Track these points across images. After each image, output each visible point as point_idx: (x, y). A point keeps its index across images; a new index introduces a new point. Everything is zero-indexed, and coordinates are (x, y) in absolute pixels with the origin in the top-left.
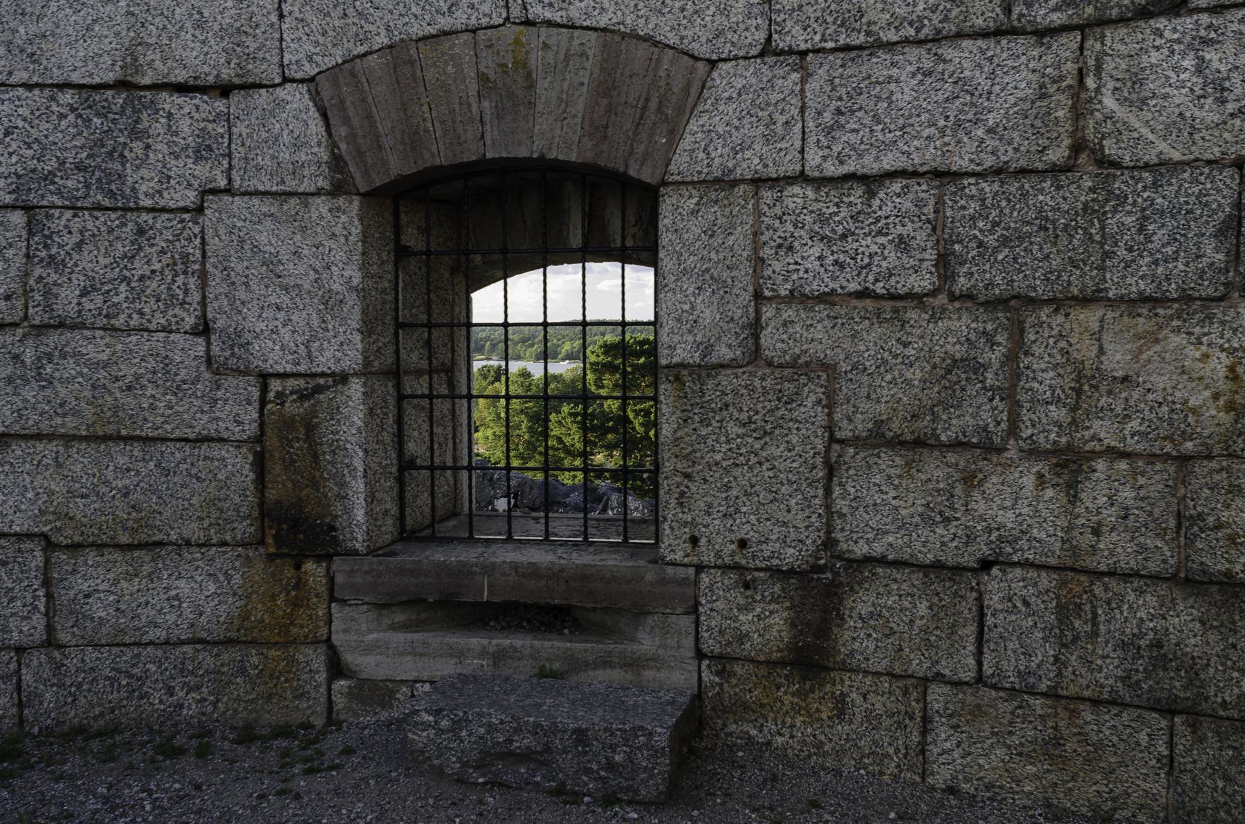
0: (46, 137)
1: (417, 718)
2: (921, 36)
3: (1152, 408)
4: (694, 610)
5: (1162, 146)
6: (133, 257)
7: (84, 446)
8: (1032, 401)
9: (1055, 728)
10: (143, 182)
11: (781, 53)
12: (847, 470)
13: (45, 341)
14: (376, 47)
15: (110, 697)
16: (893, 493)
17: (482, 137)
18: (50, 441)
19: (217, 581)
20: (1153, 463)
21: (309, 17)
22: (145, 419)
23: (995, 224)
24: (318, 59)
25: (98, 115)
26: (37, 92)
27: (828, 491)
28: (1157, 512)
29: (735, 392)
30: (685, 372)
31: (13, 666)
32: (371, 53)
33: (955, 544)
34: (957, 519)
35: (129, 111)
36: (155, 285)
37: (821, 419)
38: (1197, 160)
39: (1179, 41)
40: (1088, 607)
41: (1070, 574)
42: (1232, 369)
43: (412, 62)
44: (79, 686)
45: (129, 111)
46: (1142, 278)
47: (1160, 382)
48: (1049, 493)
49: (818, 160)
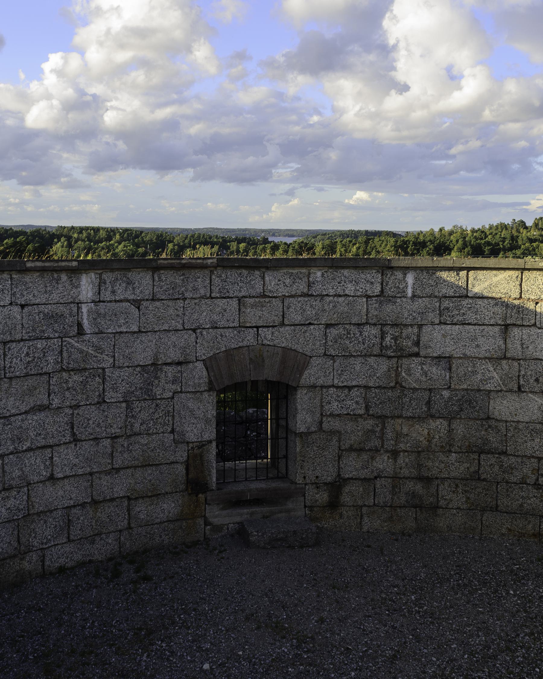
1: (252, 534)
2: (362, 355)
4: (304, 496)
5: (414, 385)
9: (391, 514)
10: (158, 392)
11: (328, 355)
13: (130, 439)
16: (354, 462)
18: (131, 468)
19: (175, 503)
21: (204, 343)
22: (157, 459)
23: (379, 399)
24: (206, 354)
25: (146, 373)
26: (130, 368)
27: (339, 462)
29: (316, 439)
30: (303, 434)
31: (118, 536)
36: (160, 420)
37: (337, 445)
39: (418, 363)
40: (399, 486)
42: (428, 433)
47: (414, 435)
48: (390, 460)
49: (337, 382)
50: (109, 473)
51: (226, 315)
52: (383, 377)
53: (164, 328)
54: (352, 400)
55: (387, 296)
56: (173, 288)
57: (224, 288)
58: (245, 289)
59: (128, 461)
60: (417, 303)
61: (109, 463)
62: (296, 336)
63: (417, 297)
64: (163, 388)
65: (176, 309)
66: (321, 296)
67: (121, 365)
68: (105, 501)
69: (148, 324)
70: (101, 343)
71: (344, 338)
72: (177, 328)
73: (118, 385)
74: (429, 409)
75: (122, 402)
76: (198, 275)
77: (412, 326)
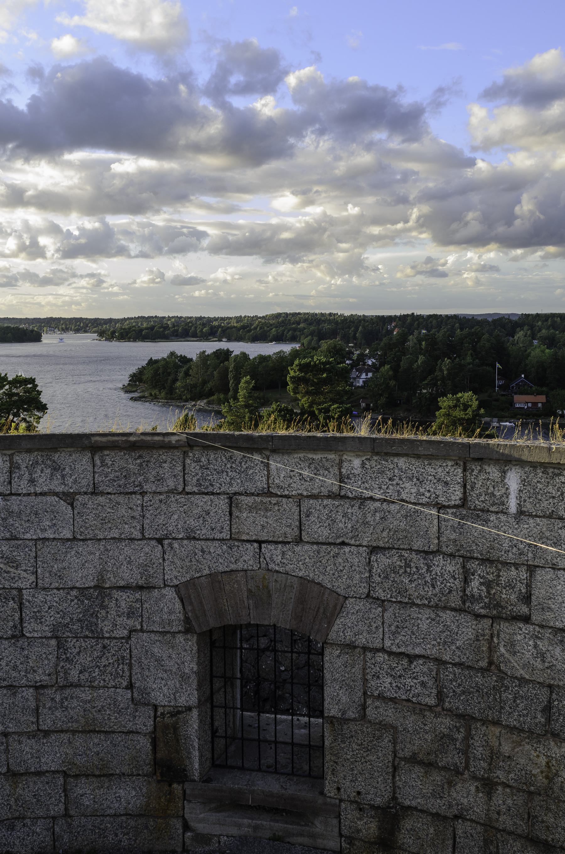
0: (65, 609)
3: (519, 771)
5: (522, 672)
6: (101, 657)
7: (80, 735)
8: (474, 757)
10: (106, 627)
11: (374, 598)
12: (402, 770)
13: (64, 692)
14: (204, 574)
15: (91, 837)
17: (249, 614)
18: (66, 733)
19: (135, 790)
20: (519, 792)
21: (176, 561)
22: (106, 724)
23: (460, 685)
24: (180, 578)
25: (87, 599)
26: (62, 591)
27: (394, 777)
28: (521, 811)
30: (334, 720)
31: (51, 825)
32: (202, 576)
33: (444, 807)
34: (445, 798)
35: (100, 598)
36: (110, 669)
37: (391, 748)
38: (535, 681)
39: (528, 634)
40: (495, 842)
41: (489, 828)
42: (547, 763)
43: (219, 582)
44: (78, 833)
45: (100, 598)
46: (515, 720)
49: (389, 645)
50: (34, 737)
51: (209, 520)
52: (467, 649)
53: (112, 536)
54: (414, 678)
55: (472, 508)
56: (125, 476)
57: (205, 479)
58: (239, 481)
59: (63, 722)
60: (526, 526)
61: (33, 723)
62: (320, 562)
63: (526, 515)
64: (113, 622)
65: (131, 508)
66: (361, 499)
67: (47, 586)
68: (30, 773)
69: (87, 528)
70: (15, 554)
71: (401, 572)
72: (133, 536)
73: (43, 614)
74: (549, 720)
75: (51, 638)
76: (164, 457)
77: (516, 566)
